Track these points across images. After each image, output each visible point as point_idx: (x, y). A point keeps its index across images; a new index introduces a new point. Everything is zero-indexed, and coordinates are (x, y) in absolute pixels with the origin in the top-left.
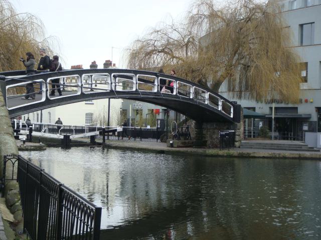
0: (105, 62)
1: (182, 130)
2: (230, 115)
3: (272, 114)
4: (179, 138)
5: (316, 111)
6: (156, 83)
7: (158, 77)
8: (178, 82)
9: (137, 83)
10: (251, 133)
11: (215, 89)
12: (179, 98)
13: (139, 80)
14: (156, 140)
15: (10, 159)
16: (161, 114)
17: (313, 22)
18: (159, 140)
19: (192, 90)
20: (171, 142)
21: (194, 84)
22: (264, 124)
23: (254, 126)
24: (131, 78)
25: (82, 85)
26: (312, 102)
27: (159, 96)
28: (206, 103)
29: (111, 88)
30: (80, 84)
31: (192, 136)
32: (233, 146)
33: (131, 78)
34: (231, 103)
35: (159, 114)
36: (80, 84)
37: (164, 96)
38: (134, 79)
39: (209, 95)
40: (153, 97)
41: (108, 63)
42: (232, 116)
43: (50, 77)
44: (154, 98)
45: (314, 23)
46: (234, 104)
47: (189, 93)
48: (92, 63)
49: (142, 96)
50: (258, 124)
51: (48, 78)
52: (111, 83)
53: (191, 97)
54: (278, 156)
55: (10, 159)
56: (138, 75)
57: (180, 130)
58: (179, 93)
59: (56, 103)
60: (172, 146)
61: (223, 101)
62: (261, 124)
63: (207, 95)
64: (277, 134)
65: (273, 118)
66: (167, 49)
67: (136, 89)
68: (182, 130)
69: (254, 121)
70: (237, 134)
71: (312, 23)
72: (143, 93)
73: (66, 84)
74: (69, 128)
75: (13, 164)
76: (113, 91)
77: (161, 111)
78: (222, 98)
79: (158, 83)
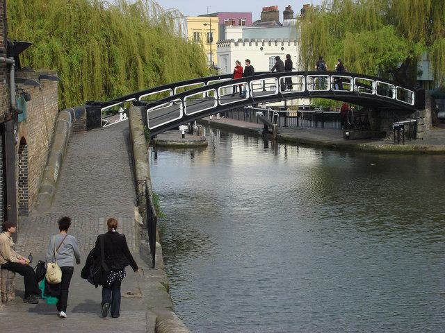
42: (413, 104)
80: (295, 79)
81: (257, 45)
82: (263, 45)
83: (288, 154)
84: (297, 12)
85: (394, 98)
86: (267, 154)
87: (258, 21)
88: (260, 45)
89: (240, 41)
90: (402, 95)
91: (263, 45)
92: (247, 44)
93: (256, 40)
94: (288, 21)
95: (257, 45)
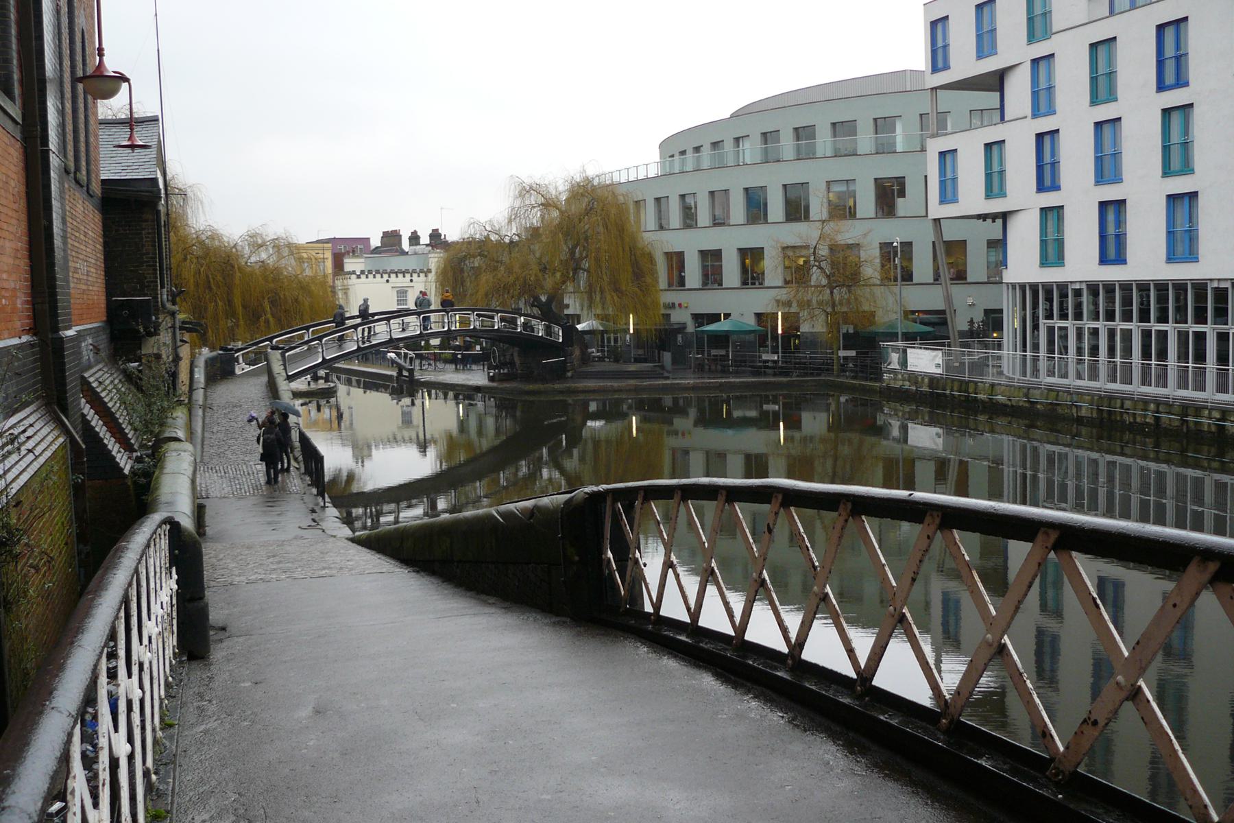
42: (561, 340)
70: (568, 361)
80: (433, 316)
81: (382, 277)
82: (389, 277)
83: (1032, 589)
84: (425, 240)
85: (540, 335)
86: (655, 156)
87: (377, 248)
88: (386, 276)
89: (363, 272)
90: (548, 330)
91: (389, 277)
92: (371, 276)
93: (381, 271)
94: (414, 247)
95: (382, 277)
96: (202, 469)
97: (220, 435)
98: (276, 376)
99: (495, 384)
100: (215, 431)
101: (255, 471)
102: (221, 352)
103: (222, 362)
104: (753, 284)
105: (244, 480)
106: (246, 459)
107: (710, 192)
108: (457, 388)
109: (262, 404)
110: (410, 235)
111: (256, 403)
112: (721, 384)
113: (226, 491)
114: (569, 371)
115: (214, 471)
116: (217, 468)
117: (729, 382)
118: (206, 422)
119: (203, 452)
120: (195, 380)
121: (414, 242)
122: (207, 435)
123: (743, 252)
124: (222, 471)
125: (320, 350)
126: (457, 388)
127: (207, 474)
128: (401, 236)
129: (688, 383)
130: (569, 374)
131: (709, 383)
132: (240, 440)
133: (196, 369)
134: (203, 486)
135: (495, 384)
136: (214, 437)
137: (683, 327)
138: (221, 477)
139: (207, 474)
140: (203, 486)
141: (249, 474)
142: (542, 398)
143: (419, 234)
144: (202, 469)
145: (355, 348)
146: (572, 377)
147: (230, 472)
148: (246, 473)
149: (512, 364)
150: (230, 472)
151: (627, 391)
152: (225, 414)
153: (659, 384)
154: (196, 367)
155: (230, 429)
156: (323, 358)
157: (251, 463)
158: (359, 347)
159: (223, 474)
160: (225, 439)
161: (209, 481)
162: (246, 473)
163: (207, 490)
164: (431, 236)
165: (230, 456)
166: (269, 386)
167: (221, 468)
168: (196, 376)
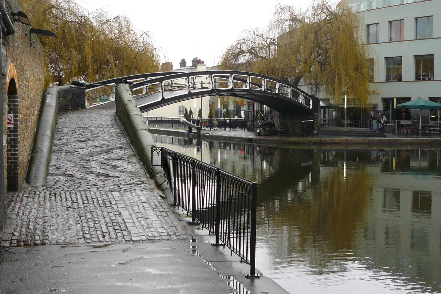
0: (193, 59)
1: (267, 120)
2: (309, 107)
3: (344, 105)
4: (265, 127)
5: (382, 101)
6: (248, 81)
7: (249, 75)
8: (279, 83)
9: (232, 82)
10: (326, 121)
11: (295, 85)
12: (267, 93)
13: (235, 78)
14: (243, 129)
15: (155, 150)
16: (245, 106)
17: (378, 22)
18: (246, 130)
19: (278, 86)
20: (258, 131)
21: (279, 81)
22: (337, 114)
23: (328, 115)
24: (228, 77)
25: (189, 86)
26: (378, 93)
27: (250, 92)
28: (289, 97)
29: (212, 87)
30: (188, 85)
31: (276, 125)
32: (313, 135)
33: (228, 77)
34: (310, 96)
35: (243, 106)
36: (188, 85)
37: (255, 92)
38: (230, 78)
39: (292, 89)
40: (246, 93)
41: (196, 62)
42: (311, 108)
43: (164, 80)
44: (246, 94)
45: (379, 23)
46: (313, 97)
47: (275, 88)
48: (182, 60)
49: (237, 93)
50: (333, 113)
51: (148, 77)
52: (212, 83)
53: (277, 92)
54: (351, 142)
55: (155, 150)
56: (233, 75)
57: (265, 120)
58: (267, 89)
59: (170, 101)
60: (259, 134)
61: (303, 95)
62: (334, 114)
63: (290, 90)
64: (349, 122)
65: (345, 107)
66: (252, 51)
67: (232, 87)
68: (267, 120)
69: (329, 110)
70: (315, 123)
71: (377, 24)
72: (238, 91)
73: (174, 85)
74: (166, 119)
75: (158, 154)
76: (214, 89)
77: (245, 103)
78: (302, 92)
79: (250, 81)
96: (42, 195)
97: (70, 157)
98: (127, 102)
99: (261, 138)
100: (63, 152)
101: (112, 200)
102: (73, 86)
103: (73, 95)
104: (424, 80)
105: (100, 213)
106: (99, 184)
107: (389, 22)
108: (234, 140)
109: (112, 129)
110: (180, 61)
111: (106, 129)
112: (431, 141)
113: (73, 232)
114: (315, 130)
115: (58, 198)
116: (63, 195)
117: (437, 140)
118: (55, 143)
119: (47, 174)
120: (46, 104)
121: (183, 65)
122: (54, 155)
123: (418, 58)
124: (69, 199)
125: (160, 90)
126: (234, 140)
127: (48, 203)
128: (172, 65)
129: (407, 140)
130: (316, 132)
131: (423, 140)
132: (91, 162)
133: (48, 96)
134: (40, 221)
135: (261, 138)
136: (62, 158)
137: (375, 107)
138: (68, 208)
139: (48, 203)
140: (40, 221)
141: (104, 204)
142: (301, 147)
143: (186, 61)
144: (42, 195)
145: (187, 93)
146: (317, 134)
147: (80, 200)
148: (101, 202)
149: (271, 124)
150: (80, 200)
151: (362, 144)
152: (75, 137)
153: (386, 140)
154: (49, 94)
155: (80, 151)
156: (163, 98)
157: (106, 189)
158: (190, 93)
159: (70, 203)
160: (74, 160)
161: (49, 214)
162: (101, 202)
163: (44, 230)
164: (193, 61)
165: (79, 180)
166: (118, 116)
167: (68, 194)
168: (48, 100)
